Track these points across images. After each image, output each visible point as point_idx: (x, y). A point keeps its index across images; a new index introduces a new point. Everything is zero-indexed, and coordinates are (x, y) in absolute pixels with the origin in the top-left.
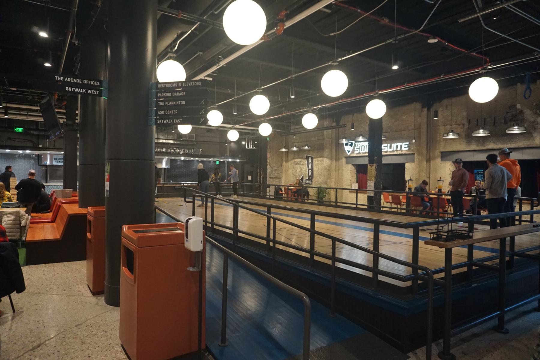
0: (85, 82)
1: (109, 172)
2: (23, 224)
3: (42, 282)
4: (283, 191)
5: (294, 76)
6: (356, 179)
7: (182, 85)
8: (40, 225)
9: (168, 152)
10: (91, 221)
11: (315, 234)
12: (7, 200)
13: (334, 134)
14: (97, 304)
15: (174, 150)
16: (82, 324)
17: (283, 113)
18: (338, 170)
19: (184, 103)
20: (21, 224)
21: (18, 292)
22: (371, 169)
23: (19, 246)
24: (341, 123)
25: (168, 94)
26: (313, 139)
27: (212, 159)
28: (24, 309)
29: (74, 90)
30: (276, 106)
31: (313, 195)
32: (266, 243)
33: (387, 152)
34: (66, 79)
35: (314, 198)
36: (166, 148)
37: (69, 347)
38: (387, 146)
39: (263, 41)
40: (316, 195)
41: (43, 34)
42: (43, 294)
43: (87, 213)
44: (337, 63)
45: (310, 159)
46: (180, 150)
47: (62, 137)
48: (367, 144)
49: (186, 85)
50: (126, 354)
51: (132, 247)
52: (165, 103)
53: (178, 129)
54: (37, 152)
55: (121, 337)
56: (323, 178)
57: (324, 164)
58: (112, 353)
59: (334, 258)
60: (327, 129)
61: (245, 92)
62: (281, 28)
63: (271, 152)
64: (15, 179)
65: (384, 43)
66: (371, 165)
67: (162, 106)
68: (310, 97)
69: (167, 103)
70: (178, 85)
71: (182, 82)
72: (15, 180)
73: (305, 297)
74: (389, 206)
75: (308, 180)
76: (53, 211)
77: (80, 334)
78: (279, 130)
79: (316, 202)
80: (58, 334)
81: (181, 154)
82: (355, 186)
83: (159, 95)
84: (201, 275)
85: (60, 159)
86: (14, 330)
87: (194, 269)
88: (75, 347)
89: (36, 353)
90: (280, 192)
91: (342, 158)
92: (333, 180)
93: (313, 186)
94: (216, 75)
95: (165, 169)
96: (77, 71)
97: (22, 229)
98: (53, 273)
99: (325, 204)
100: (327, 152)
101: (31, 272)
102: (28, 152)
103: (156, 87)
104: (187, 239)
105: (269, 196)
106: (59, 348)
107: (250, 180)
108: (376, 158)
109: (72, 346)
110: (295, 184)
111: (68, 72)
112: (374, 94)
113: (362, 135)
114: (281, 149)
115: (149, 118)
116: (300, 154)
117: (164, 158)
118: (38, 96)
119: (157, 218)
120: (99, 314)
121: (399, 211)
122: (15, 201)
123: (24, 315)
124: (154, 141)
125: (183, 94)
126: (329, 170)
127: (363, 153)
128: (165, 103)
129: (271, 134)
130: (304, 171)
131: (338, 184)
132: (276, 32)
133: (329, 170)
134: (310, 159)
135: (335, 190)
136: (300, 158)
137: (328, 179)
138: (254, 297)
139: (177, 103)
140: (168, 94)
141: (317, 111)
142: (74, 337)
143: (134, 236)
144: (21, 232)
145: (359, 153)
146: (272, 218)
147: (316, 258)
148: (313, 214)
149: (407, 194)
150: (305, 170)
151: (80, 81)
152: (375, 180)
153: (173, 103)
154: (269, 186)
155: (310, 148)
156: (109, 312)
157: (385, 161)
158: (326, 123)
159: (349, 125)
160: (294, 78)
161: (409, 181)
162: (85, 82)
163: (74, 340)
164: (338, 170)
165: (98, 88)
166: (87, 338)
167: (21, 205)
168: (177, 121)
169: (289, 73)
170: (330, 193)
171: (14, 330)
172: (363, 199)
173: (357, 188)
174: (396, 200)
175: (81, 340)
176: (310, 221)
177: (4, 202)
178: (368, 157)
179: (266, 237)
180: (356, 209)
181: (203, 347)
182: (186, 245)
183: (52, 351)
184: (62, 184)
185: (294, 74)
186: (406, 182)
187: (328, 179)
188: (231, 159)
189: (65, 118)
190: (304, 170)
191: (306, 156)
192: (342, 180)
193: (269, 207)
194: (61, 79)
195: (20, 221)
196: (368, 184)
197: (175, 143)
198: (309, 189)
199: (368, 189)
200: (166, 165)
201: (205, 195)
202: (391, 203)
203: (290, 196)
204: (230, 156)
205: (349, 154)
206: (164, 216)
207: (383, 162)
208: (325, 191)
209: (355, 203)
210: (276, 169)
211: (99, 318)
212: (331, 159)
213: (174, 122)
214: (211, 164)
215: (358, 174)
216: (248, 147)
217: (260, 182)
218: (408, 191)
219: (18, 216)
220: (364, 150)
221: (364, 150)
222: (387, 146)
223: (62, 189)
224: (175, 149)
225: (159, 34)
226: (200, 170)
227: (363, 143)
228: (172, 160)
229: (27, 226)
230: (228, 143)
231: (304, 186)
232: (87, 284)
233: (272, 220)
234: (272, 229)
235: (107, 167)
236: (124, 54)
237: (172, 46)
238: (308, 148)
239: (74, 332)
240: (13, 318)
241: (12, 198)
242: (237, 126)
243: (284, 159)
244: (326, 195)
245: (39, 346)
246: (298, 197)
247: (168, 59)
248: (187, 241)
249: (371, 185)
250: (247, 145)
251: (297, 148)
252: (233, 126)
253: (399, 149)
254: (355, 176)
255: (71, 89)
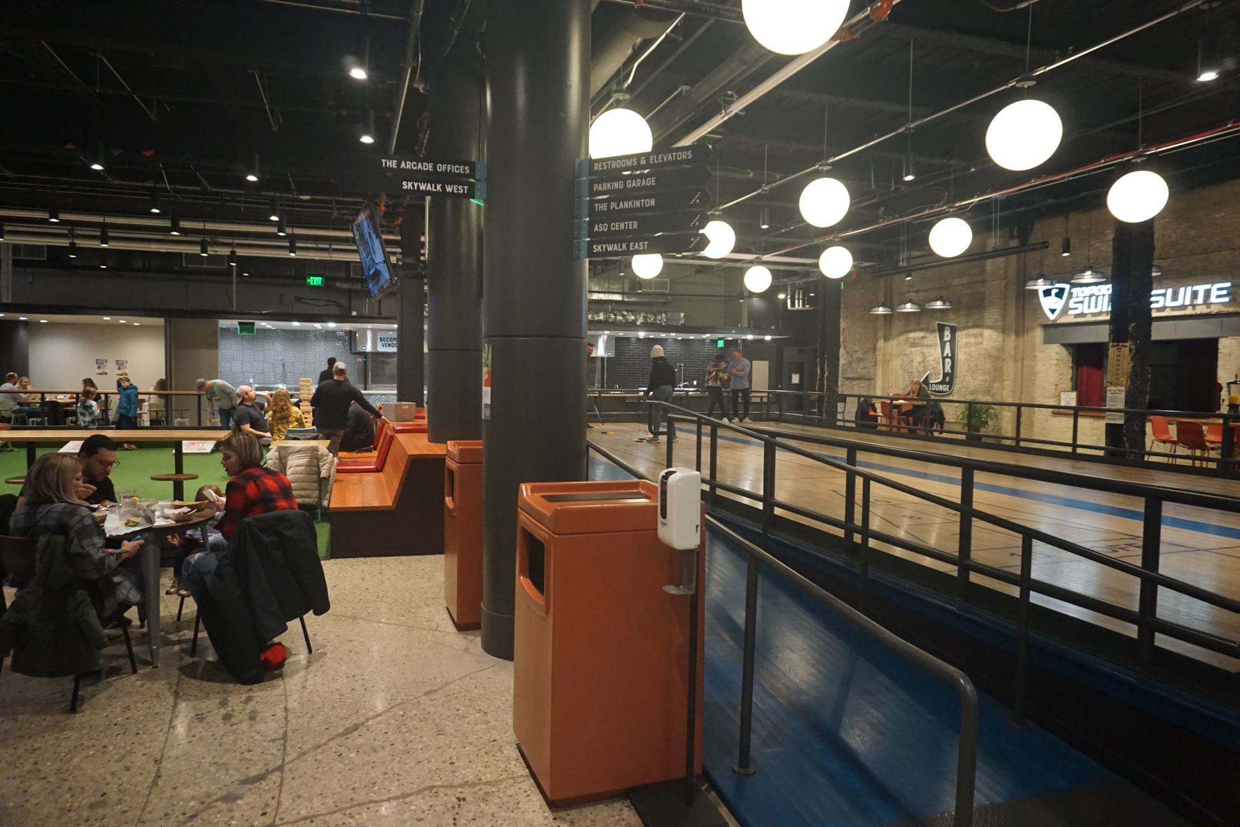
0: (441, 168)
1: (490, 364)
2: (324, 474)
3: (360, 594)
4: (879, 412)
5: (912, 125)
6: (1072, 381)
7: (648, 160)
8: (356, 477)
9: (610, 320)
10: (453, 472)
11: (974, 519)
12: (296, 423)
13: (1013, 270)
14: (466, 650)
15: (624, 316)
16: (436, 691)
17: (881, 221)
18: (1023, 358)
19: (653, 202)
20: (319, 473)
21: (318, 613)
22: (1119, 356)
23: (317, 518)
24: (1034, 238)
25: (618, 185)
26: (956, 282)
27: (708, 335)
28: (329, 647)
29: (418, 186)
30: (862, 205)
31: (953, 421)
32: (843, 536)
33: (1163, 309)
34: (403, 165)
35: (958, 428)
36: (606, 312)
37: (412, 737)
38: (1164, 295)
39: (838, 42)
40: (962, 421)
41: (359, 73)
42: (362, 619)
43: (444, 452)
44: (1033, 83)
45: (947, 333)
46: (635, 316)
47: (392, 294)
48: (1107, 290)
49: (657, 159)
50: (529, 767)
51: (542, 533)
52: (609, 206)
53: (632, 270)
54: (348, 326)
55: (517, 728)
56: (980, 378)
57: (985, 343)
58: (498, 761)
59: (1026, 582)
60: (993, 257)
61: (787, 174)
62: (885, 5)
63: (847, 317)
64: (309, 381)
65: (1176, 13)
66: (1117, 345)
67: (603, 212)
68: (952, 176)
69: (613, 205)
70: (639, 161)
71: (647, 155)
72: (308, 384)
73: (962, 681)
74: (1168, 452)
75: (942, 383)
76: (378, 449)
77: (435, 713)
78: (868, 264)
79: (963, 437)
80: (392, 708)
81: (638, 326)
82: (1070, 399)
83: (596, 187)
84: (695, 602)
85: (392, 339)
86: (310, 689)
87: (680, 589)
88: (425, 739)
89: (349, 742)
90: (872, 413)
91: (1033, 329)
92: (1008, 383)
93: (955, 398)
94: (720, 137)
95: (603, 359)
96: (423, 150)
97: (323, 483)
98: (380, 576)
99: (879, 431)
100: (992, 315)
101: (339, 573)
102: (332, 325)
103: (590, 169)
104: (663, 520)
105: (844, 421)
106: (392, 738)
107: (796, 385)
108: (1133, 325)
109: (417, 736)
110: (908, 394)
111: (407, 149)
112: (1133, 159)
113: (1090, 268)
114: (874, 310)
115: (575, 241)
116: (921, 319)
117: (600, 336)
118: (348, 209)
119: (590, 469)
120: (471, 674)
121: (1198, 463)
122: (309, 426)
123: (327, 660)
124: (586, 296)
125: (651, 182)
126: (997, 358)
127: (1094, 315)
128: (609, 206)
129: (850, 273)
130: (932, 362)
131: (1022, 393)
132: (871, 17)
133: (997, 358)
134: (947, 333)
135: (1015, 409)
136: (921, 330)
137: (994, 380)
138: (814, 662)
139: (638, 204)
140: (618, 185)
141: (969, 211)
142: (422, 717)
143: (546, 509)
144: (320, 491)
145: (1083, 315)
146: (861, 474)
147: (975, 578)
148: (969, 468)
149: (1224, 421)
150: (934, 360)
151: (430, 167)
152: (1129, 383)
153: (627, 205)
154: (843, 398)
155: (947, 303)
156: (491, 670)
157: (1159, 333)
158: (993, 242)
159: (1057, 242)
160: (912, 131)
161: (1232, 385)
162: (441, 168)
163: (422, 723)
164: (1023, 359)
165: (466, 180)
166: (448, 723)
167: (321, 435)
168: (636, 246)
169: (901, 119)
170: (1000, 417)
171: (310, 689)
172: (1092, 432)
173: (1074, 404)
174: (1191, 437)
175: (436, 725)
176: (960, 487)
177: (291, 427)
178: (1110, 325)
179: (843, 519)
180: (1074, 456)
181: (697, 770)
182: (662, 533)
183: (380, 743)
184: (396, 392)
185: (912, 122)
186: (1221, 388)
187: (994, 380)
188: (753, 334)
189: (400, 253)
190: (932, 358)
191: (939, 324)
192: (1034, 384)
193: (853, 449)
194: (392, 164)
195: (318, 466)
196: (1108, 392)
197: (626, 300)
198: (945, 407)
199: (1107, 407)
200: (607, 349)
201: (696, 418)
202: (1174, 442)
203: (895, 423)
204: (749, 327)
205: (1052, 317)
206: (602, 463)
207: (1155, 336)
208: (987, 410)
209: (1071, 442)
210: (861, 356)
211: (472, 681)
212: (1004, 331)
213: (631, 249)
214: (707, 349)
215: (1077, 369)
216: (793, 305)
217: (821, 389)
218: (1229, 411)
219: (315, 457)
220: (1096, 307)
221: (1096, 307)
222: (1164, 295)
223: (395, 402)
224: (625, 313)
225: (595, 49)
226: (656, 359)
227: (1093, 287)
228: (618, 339)
229: (331, 478)
230: (746, 297)
231: (933, 397)
232: (445, 605)
233: (859, 481)
234: (861, 504)
235: (487, 355)
236: (521, 99)
237: (621, 77)
238: (944, 304)
239: (422, 706)
240: (309, 663)
241: (304, 420)
242: (766, 258)
243: (881, 333)
244: (989, 420)
245: (356, 728)
246: (915, 424)
247: (611, 107)
248: (664, 524)
249: (1116, 397)
250: (789, 301)
251: (915, 306)
252: (757, 258)
253: (1200, 300)
254: (1068, 373)
255: (413, 186)
